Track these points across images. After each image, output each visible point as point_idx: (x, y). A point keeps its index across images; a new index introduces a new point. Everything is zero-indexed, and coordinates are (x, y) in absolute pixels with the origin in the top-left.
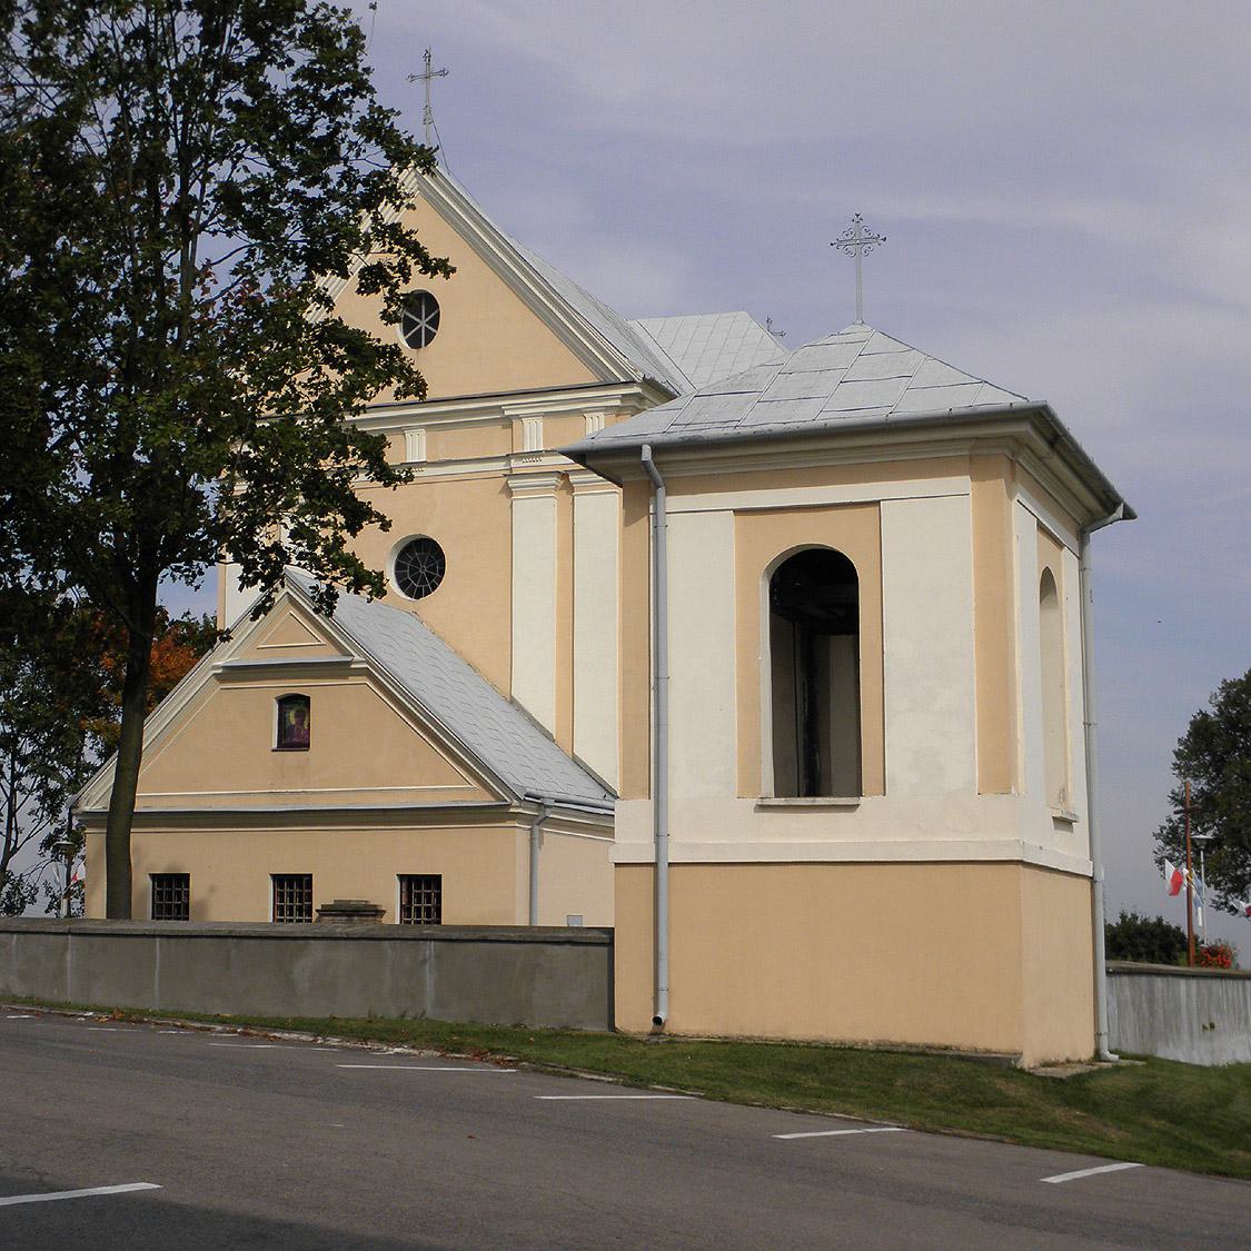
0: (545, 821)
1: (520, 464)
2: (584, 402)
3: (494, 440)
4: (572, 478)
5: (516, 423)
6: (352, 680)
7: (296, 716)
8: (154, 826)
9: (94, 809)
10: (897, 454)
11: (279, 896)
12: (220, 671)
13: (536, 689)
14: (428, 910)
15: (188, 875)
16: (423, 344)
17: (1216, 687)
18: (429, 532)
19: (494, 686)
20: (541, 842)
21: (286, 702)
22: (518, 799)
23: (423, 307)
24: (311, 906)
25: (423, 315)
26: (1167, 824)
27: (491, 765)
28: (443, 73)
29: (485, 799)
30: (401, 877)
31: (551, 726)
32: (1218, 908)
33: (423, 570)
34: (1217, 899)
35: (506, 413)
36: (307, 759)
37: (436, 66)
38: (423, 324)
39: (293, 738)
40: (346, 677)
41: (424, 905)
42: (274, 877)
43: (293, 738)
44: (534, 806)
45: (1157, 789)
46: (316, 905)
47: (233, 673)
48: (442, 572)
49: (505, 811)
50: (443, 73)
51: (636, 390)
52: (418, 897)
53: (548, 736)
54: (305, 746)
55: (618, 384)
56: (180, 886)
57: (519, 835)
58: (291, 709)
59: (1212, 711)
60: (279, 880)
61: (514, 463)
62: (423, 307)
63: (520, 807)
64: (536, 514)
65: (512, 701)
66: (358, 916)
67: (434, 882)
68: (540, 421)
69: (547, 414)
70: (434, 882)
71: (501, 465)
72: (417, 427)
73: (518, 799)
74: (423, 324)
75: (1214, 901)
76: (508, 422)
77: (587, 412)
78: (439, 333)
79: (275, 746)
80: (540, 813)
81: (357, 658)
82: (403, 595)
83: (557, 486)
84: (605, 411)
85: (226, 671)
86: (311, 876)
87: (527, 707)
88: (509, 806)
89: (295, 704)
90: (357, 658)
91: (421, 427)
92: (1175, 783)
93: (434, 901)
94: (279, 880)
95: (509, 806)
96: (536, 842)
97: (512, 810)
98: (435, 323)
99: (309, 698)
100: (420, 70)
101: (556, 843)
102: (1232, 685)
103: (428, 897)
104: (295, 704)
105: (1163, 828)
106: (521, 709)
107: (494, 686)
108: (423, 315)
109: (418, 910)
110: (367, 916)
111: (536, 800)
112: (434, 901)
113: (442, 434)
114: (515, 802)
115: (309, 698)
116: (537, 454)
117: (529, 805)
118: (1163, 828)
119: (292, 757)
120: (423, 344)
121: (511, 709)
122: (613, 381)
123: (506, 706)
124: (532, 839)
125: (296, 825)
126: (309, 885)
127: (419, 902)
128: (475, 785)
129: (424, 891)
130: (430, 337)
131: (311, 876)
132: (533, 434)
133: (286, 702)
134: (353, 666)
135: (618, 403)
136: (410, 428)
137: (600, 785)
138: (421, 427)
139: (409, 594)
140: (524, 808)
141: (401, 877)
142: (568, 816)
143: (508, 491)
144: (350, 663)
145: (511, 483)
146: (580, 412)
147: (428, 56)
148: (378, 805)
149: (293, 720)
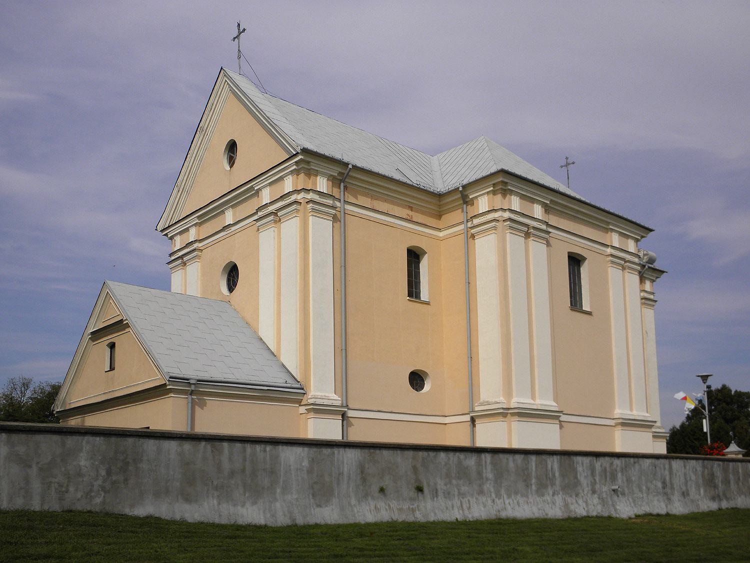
2: (283, 171)
3: (250, 207)
51: (300, 157)
53: (273, 353)
64: (267, 237)
69: (271, 184)
84: (291, 174)
97: (168, 387)
134: (124, 323)
135: (295, 167)
140: (172, 385)
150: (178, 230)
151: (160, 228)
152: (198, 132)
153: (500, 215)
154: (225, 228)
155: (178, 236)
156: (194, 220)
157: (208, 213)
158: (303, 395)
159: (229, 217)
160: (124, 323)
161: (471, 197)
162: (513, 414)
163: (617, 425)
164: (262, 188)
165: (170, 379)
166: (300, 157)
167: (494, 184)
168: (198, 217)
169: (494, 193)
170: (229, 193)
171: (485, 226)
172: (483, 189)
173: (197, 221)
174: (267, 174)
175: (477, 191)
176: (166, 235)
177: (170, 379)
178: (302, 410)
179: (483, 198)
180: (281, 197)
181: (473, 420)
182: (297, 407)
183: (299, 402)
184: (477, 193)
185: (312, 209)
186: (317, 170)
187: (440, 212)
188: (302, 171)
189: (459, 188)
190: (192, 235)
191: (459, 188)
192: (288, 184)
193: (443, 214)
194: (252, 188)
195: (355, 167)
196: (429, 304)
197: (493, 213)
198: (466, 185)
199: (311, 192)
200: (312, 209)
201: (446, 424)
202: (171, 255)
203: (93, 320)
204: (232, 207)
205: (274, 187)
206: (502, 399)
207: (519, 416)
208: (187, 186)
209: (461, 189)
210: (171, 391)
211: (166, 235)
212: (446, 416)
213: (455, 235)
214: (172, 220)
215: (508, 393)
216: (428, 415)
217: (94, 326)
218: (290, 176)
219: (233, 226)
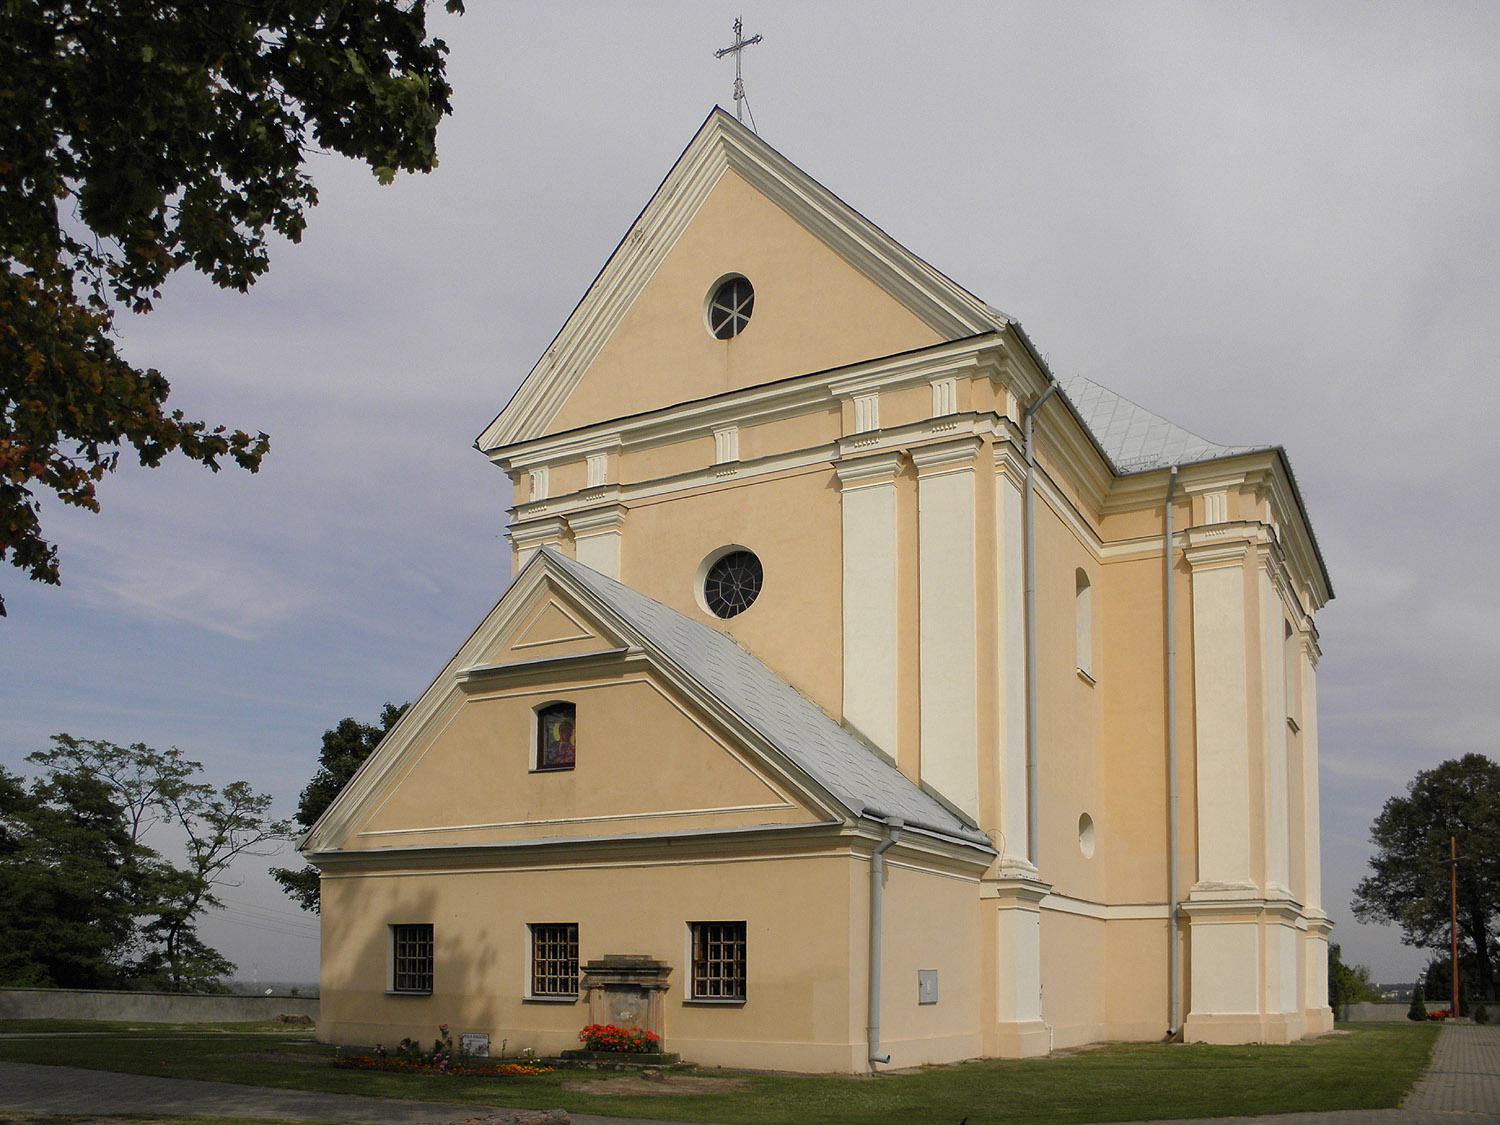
0: (889, 849)
1: (852, 449)
2: (934, 366)
3: (821, 427)
4: (916, 458)
5: (845, 404)
6: (628, 678)
7: (561, 731)
8: (394, 869)
9: (327, 850)
11: (539, 950)
12: (466, 679)
13: (873, 709)
14: (729, 967)
15: (745, 922)
16: (735, 331)
17: (1412, 777)
18: (746, 541)
19: (822, 709)
20: (885, 873)
21: (546, 712)
22: (854, 816)
23: (735, 295)
24: (577, 964)
25: (735, 303)
26: (1364, 883)
27: (815, 773)
28: (756, 40)
29: (809, 820)
30: (693, 925)
31: (891, 748)
32: (1407, 944)
33: (737, 587)
34: (1405, 937)
35: (834, 393)
37: (747, 35)
38: (735, 314)
39: (555, 757)
40: (619, 675)
41: (723, 960)
42: (533, 927)
43: (555, 757)
44: (876, 828)
45: (1364, 853)
46: (583, 962)
48: (759, 588)
49: (832, 834)
50: (756, 40)
51: (997, 342)
52: (716, 949)
53: (888, 761)
54: (570, 765)
56: (425, 939)
57: (852, 867)
58: (553, 723)
60: (539, 930)
61: (844, 450)
62: (735, 295)
63: (856, 827)
64: (871, 509)
65: (844, 724)
66: (632, 974)
67: (737, 930)
68: (875, 398)
69: (884, 389)
70: (737, 930)
71: (829, 455)
73: (854, 816)
74: (735, 314)
75: (1403, 939)
76: (836, 404)
77: (933, 379)
78: (751, 321)
79: (533, 766)
80: (882, 839)
82: (714, 615)
83: (897, 471)
84: (957, 375)
86: (576, 925)
87: (863, 728)
88: (840, 827)
89: (557, 714)
92: (1377, 851)
93: (737, 954)
94: (539, 930)
95: (840, 827)
96: (879, 876)
97: (844, 833)
98: (748, 311)
99: (574, 705)
101: (906, 883)
102: (1427, 775)
103: (729, 949)
104: (557, 714)
105: (1361, 886)
106: (854, 733)
107: (822, 709)
108: (735, 303)
109: (716, 967)
110: (644, 974)
111: (873, 817)
112: (737, 954)
113: (758, 429)
114: (849, 822)
115: (574, 705)
116: (872, 435)
117: (868, 826)
118: (1361, 886)
119: (553, 778)
120: (735, 331)
121: (843, 736)
122: (972, 334)
123: (838, 729)
124: (872, 872)
125: (557, 863)
126: (575, 937)
127: (717, 956)
128: (791, 802)
129: (723, 942)
130: (742, 325)
131: (576, 925)
132: (867, 413)
133: (546, 712)
134: (628, 659)
135: (974, 361)
136: (719, 426)
137: (955, 816)
139: (714, 607)
140: (862, 830)
141: (693, 925)
142: (921, 844)
143: (837, 483)
145: (842, 472)
146: (925, 381)
147: (738, 26)
149: (556, 735)
150: (546, 454)
151: (486, 443)
152: (628, 242)
153: (1254, 534)
154: (713, 469)
155: (546, 470)
156: (612, 437)
157: (641, 431)
158: (992, 857)
159: (728, 445)
160: (628, 659)
161: (1187, 490)
162: (1270, 912)
163: (1311, 929)
164: (855, 395)
165: (865, 816)
166: (997, 342)
167: (1248, 473)
168: (624, 434)
169: (1242, 489)
170: (739, 393)
171: (1203, 553)
172: (1216, 479)
173: (619, 442)
174: (878, 366)
175: (1204, 481)
176: (504, 463)
177: (865, 816)
178: (990, 890)
179: (1216, 497)
180: (926, 421)
181: (1181, 920)
182: (975, 882)
183: (980, 872)
184: (1196, 485)
185: (1006, 460)
186: (1012, 379)
187: (1102, 508)
188: (988, 374)
189: (1171, 468)
190: (598, 471)
191: (1171, 468)
192: (945, 397)
193: (1108, 515)
194: (825, 388)
195: (1059, 394)
196: (1092, 685)
197: (1240, 529)
198: (1183, 465)
199: (1002, 421)
200: (1006, 460)
201: (1105, 920)
202: (515, 510)
203: (481, 641)
204: (740, 423)
205: (890, 396)
206: (1250, 882)
207: (1283, 916)
208: (577, 359)
209: (1174, 471)
210: (848, 841)
211: (504, 463)
212: (1107, 906)
213: (1142, 558)
214: (530, 432)
215: (1259, 868)
216: (1092, 903)
217: (480, 658)
218: (952, 381)
219: (741, 468)
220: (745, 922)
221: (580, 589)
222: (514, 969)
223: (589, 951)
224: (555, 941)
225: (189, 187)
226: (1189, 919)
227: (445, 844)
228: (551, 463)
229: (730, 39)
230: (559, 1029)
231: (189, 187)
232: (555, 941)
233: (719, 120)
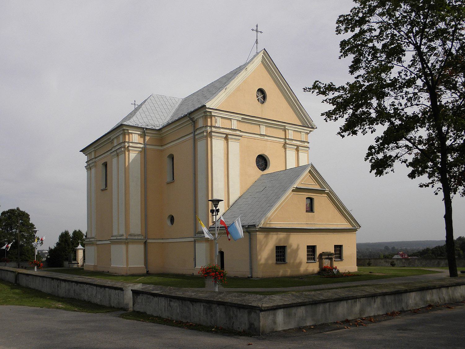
6: (323, 195)
10: (133, 130)
12: (295, 189)
15: (335, 245)
36: (314, 215)
39: (310, 208)
43: (310, 208)
47: (298, 190)
55: (309, 127)
59: (71, 234)
67: (341, 247)
68: (292, 131)
69: (294, 130)
72: (264, 125)
81: (327, 189)
85: (296, 189)
90: (327, 189)
91: (264, 125)
94: (308, 247)
100: (255, 32)
116: (219, 128)
134: (326, 191)
138: (264, 125)
144: (325, 190)
146: (300, 132)
148: (326, 227)
156: (240, 117)
190: (235, 125)
204: (266, 126)
205: (295, 132)
220: (335, 245)
221: (318, 175)
222: (303, 255)
223: (318, 252)
224: (312, 249)
225: (402, 123)
226: (85, 245)
227: (320, 227)
228: (222, 118)
229: (259, 30)
230: (314, 267)
231: (402, 123)
232: (312, 249)
233: (264, 51)
